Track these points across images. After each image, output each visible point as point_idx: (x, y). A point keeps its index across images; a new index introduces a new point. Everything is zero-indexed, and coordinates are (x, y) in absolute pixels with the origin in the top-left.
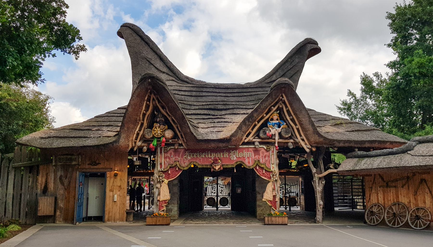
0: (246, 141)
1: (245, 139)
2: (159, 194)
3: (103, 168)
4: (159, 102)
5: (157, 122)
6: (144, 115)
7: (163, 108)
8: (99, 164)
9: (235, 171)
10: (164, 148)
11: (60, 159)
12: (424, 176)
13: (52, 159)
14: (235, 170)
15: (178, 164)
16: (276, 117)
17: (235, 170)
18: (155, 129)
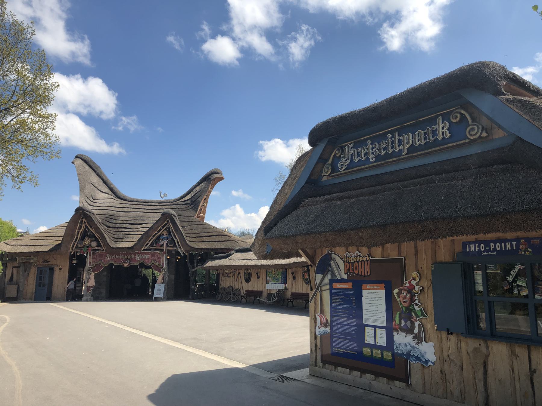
4: (88, 224)
5: (87, 236)
6: (78, 232)
7: (91, 228)
16: (165, 233)
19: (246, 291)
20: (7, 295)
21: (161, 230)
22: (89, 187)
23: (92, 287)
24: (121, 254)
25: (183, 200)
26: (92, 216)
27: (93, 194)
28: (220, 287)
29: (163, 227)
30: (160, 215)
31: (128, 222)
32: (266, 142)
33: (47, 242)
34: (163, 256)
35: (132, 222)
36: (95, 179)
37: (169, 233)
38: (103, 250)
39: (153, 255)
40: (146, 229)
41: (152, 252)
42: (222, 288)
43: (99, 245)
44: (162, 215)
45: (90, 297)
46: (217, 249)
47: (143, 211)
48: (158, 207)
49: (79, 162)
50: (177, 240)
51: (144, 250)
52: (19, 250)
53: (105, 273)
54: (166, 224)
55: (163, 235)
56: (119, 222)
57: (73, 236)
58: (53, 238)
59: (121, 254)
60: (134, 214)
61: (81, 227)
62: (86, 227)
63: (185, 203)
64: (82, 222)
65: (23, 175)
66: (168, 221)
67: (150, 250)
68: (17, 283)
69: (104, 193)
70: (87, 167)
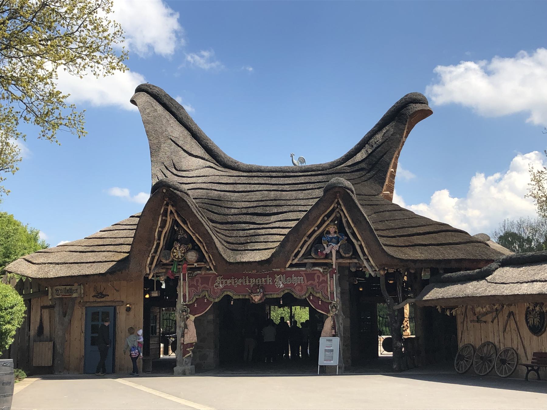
0: (296, 261)
1: (293, 260)
2: (183, 336)
3: (113, 301)
4: (179, 215)
5: (178, 241)
6: (160, 233)
7: (185, 223)
8: (106, 295)
9: (232, 303)
10: (189, 274)
11: (57, 290)
12: (512, 308)
13: (48, 290)
14: (281, 302)
15: (207, 294)
16: (332, 229)
17: (281, 302)
18: (175, 251)
19: (535, 354)
20: (37, 362)
21: (323, 221)
22: (167, 148)
23: (191, 345)
24: (246, 275)
25: (350, 162)
26: (185, 198)
27: (176, 160)
28: (460, 345)
29: (328, 216)
30: (320, 193)
31: (251, 211)
32: (451, 68)
33: (100, 257)
34: (332, 277)
35: (259, 210)
36: (177, 131)
37: (341, 229)
38: (211, 269)
39: (310, 277)
40: (293, 224)
41: (309, 271)
42: (466, 346)
43: (201, 258)
44: (326, 191)
45: (189, 367)
46: (449, 261)
47: (275, 188)
48: (302, 180)
49: (144, 98)
50: (359, 242)
51: (291, 266)
52: (53, 272)
53: (211, 317)
54: (333, 210)
55: (328, 233)
56: (233, 211)
57: (150, 242)
58: (111, 248)
59: (246, 275)
60: (258, 196)
61: (164, 222)
62: (175, 222)
63: (356, 168)
64: (166, 211)
65: (56, 115)
66: (338, 203)
67: (304, 265)
68: (51, 339)
69: (196, 157)
70: (160, 109)
